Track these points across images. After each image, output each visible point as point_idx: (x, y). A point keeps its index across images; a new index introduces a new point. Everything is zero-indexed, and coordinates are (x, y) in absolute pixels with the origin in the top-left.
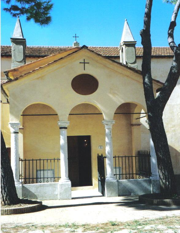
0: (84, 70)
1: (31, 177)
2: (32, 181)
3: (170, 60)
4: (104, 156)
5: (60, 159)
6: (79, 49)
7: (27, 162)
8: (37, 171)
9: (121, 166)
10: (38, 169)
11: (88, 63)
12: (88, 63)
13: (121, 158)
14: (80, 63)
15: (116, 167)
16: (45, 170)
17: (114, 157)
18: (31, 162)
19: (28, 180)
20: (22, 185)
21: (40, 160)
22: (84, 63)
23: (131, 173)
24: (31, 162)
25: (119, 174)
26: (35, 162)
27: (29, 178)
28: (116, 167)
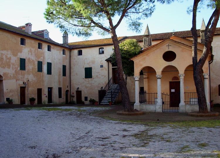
7: (186, 94)
10: (192, 98)
22: (169, 46)
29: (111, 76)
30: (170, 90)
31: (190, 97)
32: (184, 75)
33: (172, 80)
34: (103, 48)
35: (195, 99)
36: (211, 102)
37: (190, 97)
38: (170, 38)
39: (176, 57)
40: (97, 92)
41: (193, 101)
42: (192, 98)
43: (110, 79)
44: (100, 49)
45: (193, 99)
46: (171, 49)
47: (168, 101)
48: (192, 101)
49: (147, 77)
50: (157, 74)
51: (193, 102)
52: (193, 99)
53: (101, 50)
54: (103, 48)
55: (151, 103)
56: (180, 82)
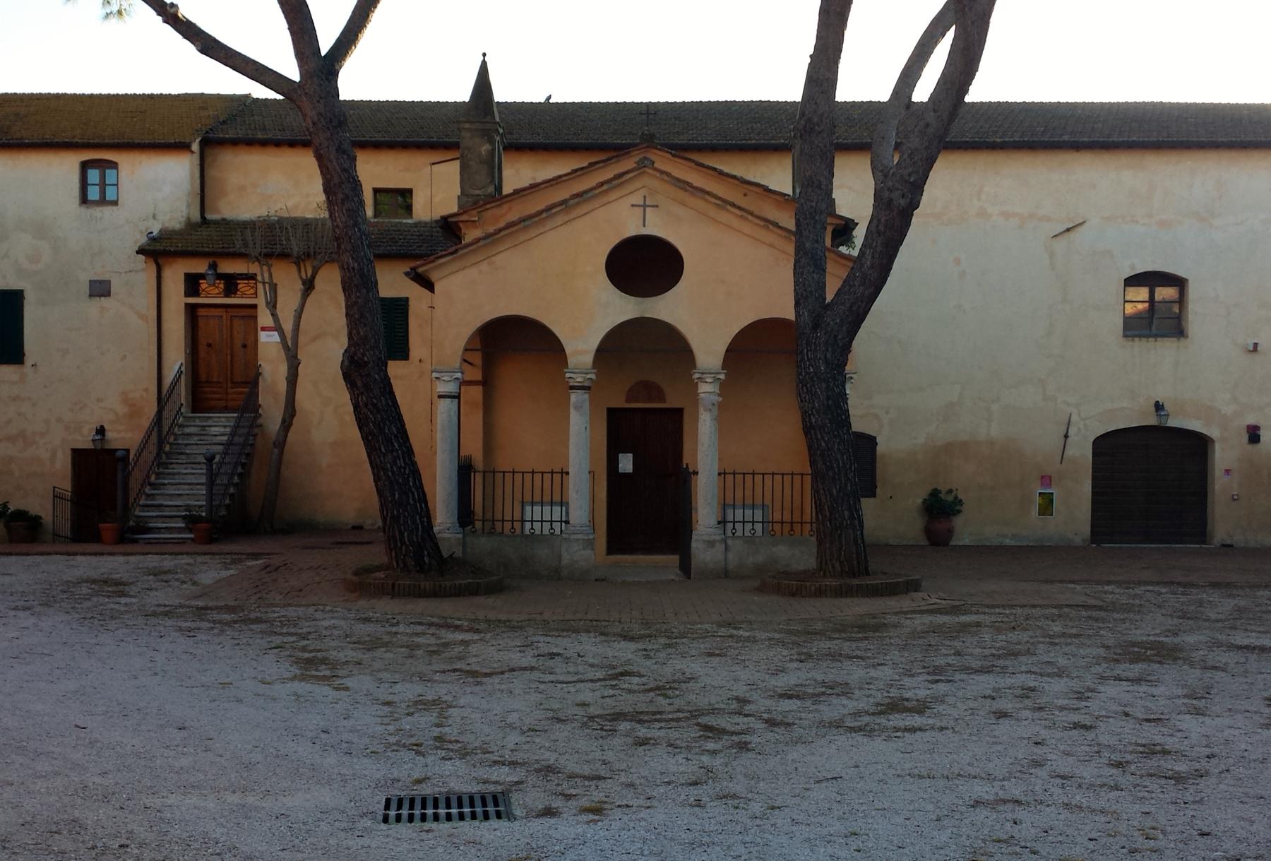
0: (644, 226)
1: (508, 517)
2: (511, 527)
3: (1148, 342)
4: (691, 470)
5: (567, 473)
6: (327, 38)
7: (730, 478)
8: (523, 504)
9: (768, 502)
10: (528, 498)
11: (657, 206)
12: (657, 206)
13: (800, 476)
14: (633, 206)
15: (753, 505)
16: (555, 503)
17: (719, 474)
18: (749, 478)
19: (501, 523)
20: (464, 536)
21: (533, 472)
22: (645, 206)
23: (797, 518)
24: (749, 478)
25: (792, 523)
26: (758, 478)
27: (503, 521)
28: (753, 505)
29: (176, 359)
30: (612, 462)
31: (518, 496)
32: (722, 377)
33: (628, 401)
34: (114, 165)
35: (748, 512)
36: (141, 538)
37: (518, 496)
38: (656, 165)
39: (608, 257)
40: (63, 463)
41: (547, 517)
42: (734, 507)
43: (169, 378)
44: (85, 166)
45: (739, 512)
46: (656, 227)
47: (807, 518)
48: (528, 516)
49: (1070, 452)
50: (571, 361)
51: (508, 525)
52: (739, 512)
53: (93, 175)
54: (114, 165)
55: (787, 527)
56: (676, 416)
